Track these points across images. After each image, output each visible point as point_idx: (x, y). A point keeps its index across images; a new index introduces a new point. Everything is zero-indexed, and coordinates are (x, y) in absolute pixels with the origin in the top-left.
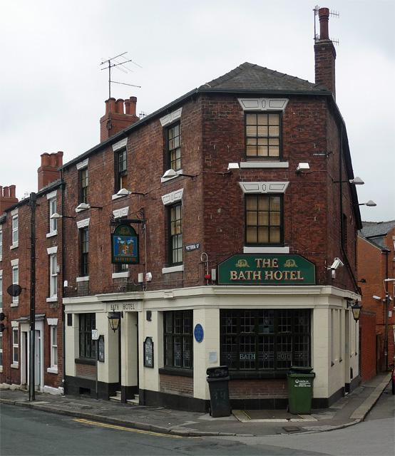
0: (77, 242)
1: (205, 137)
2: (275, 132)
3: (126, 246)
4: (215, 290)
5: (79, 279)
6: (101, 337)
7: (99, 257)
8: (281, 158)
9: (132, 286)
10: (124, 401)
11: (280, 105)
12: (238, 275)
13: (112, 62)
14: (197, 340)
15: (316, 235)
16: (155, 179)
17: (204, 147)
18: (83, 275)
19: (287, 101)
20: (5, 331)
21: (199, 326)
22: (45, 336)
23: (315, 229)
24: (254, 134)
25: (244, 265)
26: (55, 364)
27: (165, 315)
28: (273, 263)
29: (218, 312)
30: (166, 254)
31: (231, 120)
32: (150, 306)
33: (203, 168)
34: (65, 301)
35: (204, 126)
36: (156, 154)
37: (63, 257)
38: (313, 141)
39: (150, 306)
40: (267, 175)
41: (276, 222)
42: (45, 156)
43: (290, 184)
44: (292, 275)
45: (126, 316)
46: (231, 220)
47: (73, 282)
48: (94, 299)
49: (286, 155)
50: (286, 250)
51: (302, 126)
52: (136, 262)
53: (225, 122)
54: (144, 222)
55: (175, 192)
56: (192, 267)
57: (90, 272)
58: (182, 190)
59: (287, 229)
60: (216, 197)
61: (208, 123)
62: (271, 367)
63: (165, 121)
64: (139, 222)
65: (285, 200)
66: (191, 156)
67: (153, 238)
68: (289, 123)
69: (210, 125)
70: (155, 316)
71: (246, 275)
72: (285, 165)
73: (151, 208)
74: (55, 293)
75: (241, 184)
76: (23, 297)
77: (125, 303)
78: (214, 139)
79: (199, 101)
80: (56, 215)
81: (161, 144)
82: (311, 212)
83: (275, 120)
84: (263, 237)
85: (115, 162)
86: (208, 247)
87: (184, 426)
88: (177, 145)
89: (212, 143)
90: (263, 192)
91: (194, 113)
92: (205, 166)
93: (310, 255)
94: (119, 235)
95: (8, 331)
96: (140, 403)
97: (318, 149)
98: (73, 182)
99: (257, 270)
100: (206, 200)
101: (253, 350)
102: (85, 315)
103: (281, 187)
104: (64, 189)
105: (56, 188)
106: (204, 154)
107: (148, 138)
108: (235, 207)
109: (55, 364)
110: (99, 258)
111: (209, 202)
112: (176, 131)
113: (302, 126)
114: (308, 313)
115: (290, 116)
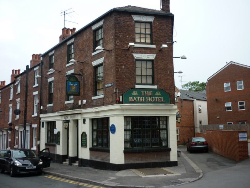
0: (48, 88)
1: (116, 31)
2: (148, 32)
3: (73, 87)
4: (122, 107)
5: (48, 105)
6: (59, 133)
7: (59, 94)
8: (152, 43)
9: (75, 106)
10: (70, 164)
11: (151, 19)
12: (133, 99)
13: (66, 12)
14: (112, 132)
15: (169, 80)
16: (88, 55)
17: (116, 36)
18: (50, 103)
19: (154, 18)
20: (12, 131)
21: (113, 126)
22: (30, 133)
23: (169, 77)
24: (139, 32)
25: (136, 94)
26: (35, 146)
27: (93, 120)
28: (150, 93)
29: (123, 119)
30: (94, 90)
31: (129, 24)
32: (85, 116)
33: (115, 46)
34: (41, 116)
35: (116, 27)
36: (89, 43)
37: (40, 96)
38: (166, 36)
39: (85, 116)
40: (146, 51)
41: (150, 72)
42: (33, 55)
43: (156, 56)
44: (159, 99)
45: (72, 122)
46: (129, 72)
47: (45, 107)
48: (56, 114)
49: (154, 42)
50: (155, 87)
51: (161, 29)
52: (78, 95)
53: (125, 25)
54: (83, 76)
55: (100, 59)
56: (109, 95)
57: (54, 102)
58: (103, 58)
59: (156, 77)
60: (122, 60)
61: (118, 25)
62: (149, 146)
63: (94, 27)
64: (80, 75)
65: (155, 63)
66: (108, 41)
67: (87, 83)
68: (155, 27)
69: (119, 26)
70: (88, 121)
71: (137, 99)
72: (154, 46)
73: (86, 68)
74: (36, 113)
75: (134, 54)
76: (21, 115)
77: (71, 115)
78: (120, 33)
79: (113, 15)
80: (38, 76)
81: (92, 38)
82: (167, 69)
83: (148, 26)
84: (144, 81)
85: (68, 50)
86: (118, 85)
87: (110, 181)
88: (100, 38)
89: (120, 35)
90: (144, 59)
91: (110, 21)
92: (116, 45)
93: (167, 89)
94: (70, 81)
95: (13, 131)
96: (79, 166)
97: (168, 40)
98: (47, 62)
99: (142, 96)
100: (117, 62)
101: (140, 137)
102: (51, 122)
103: (152, 57)
104: (42, 65)
105: (39, 65)
106: (116, 40)
107: (85, 37)
108: (131, 65)
109: (35, 146)
110: (58, 95)
111: (118, 63)
112: (100, 31)
113: (161, 29)
114: (166, 118)
115: (156, 25)
